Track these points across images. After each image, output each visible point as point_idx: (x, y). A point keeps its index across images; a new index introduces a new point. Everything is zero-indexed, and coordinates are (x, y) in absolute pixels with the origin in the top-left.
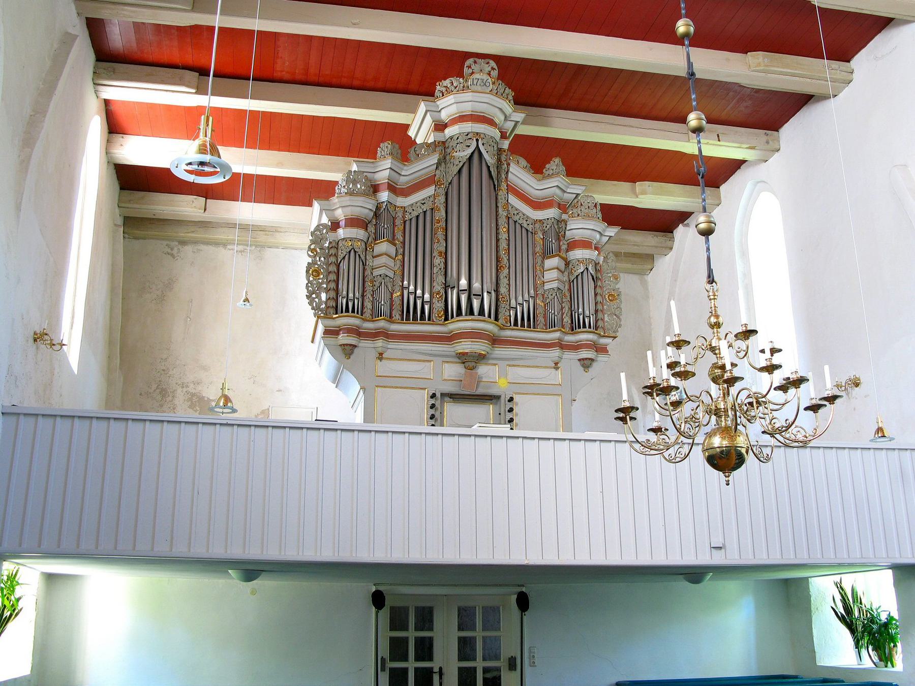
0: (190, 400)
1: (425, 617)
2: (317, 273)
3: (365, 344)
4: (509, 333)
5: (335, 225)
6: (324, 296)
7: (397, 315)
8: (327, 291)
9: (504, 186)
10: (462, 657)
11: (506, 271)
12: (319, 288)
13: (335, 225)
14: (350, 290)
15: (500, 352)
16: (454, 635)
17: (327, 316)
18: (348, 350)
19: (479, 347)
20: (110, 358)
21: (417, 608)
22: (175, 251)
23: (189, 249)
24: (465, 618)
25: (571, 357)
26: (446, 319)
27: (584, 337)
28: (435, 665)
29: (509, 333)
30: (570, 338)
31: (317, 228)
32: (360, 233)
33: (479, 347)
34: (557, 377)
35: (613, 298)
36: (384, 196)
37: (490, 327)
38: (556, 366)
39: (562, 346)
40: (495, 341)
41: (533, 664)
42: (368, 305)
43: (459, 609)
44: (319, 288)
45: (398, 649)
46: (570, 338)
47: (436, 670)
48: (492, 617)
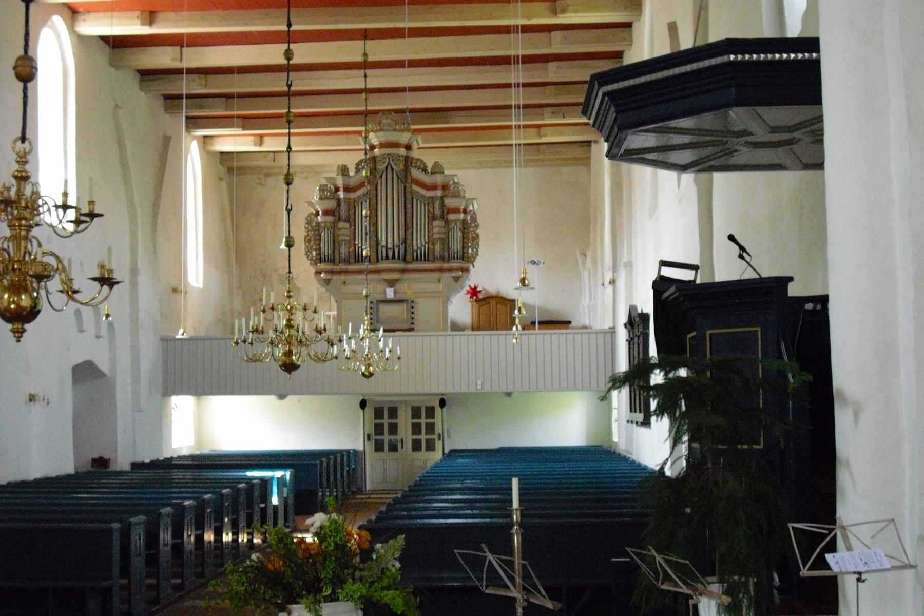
0: (281, 279)
1: (393, 412)
2: (309, 241)
3: (336, 277)
4: (411, 266)
5: (317, 214)
6: (314, 253)
7: (352, 260)
8: (316, 250)
9: (409, 178)
10: (414, 433)
11: (410, 230)
12: (311, 248)
13: (372, 147)
14: (326, 249)
15: (406, 276)
16: (410, 421)
17: (316, 264)
18: (327, 282)
19: (395, 276)
20: (228, 260)
21: (426, 407)
22: (263, 182)
23: (271, 178)
24: (416, 412)
25: (447, 275)
26: (378, 261)
27: (455, 264)
28: (398, 437)
29: (411, 266)
30: (446, 265)
31: (309, 216)
32: (330, 219)
33: (395, 276)
34: (440, 287)
35: (474, 239)
36: (341, 195)
37: (400, 265)
38: (439, 281)
39: (441, 270)
40: (403, 271)
41: (449, 437)
42: (337, 256)
43: (375, 408)
44: (311, 248)
45: (379, 429)
46: (446, 265)
47: (399, 440)
48: (431, 412)
